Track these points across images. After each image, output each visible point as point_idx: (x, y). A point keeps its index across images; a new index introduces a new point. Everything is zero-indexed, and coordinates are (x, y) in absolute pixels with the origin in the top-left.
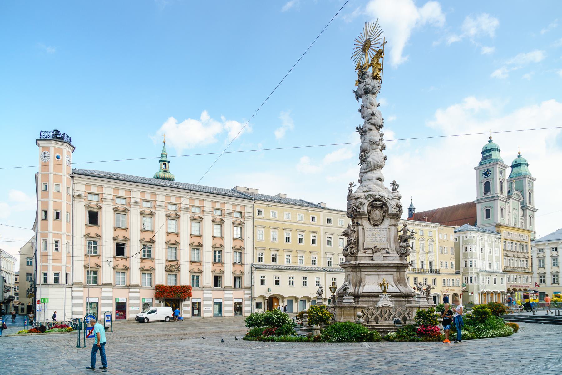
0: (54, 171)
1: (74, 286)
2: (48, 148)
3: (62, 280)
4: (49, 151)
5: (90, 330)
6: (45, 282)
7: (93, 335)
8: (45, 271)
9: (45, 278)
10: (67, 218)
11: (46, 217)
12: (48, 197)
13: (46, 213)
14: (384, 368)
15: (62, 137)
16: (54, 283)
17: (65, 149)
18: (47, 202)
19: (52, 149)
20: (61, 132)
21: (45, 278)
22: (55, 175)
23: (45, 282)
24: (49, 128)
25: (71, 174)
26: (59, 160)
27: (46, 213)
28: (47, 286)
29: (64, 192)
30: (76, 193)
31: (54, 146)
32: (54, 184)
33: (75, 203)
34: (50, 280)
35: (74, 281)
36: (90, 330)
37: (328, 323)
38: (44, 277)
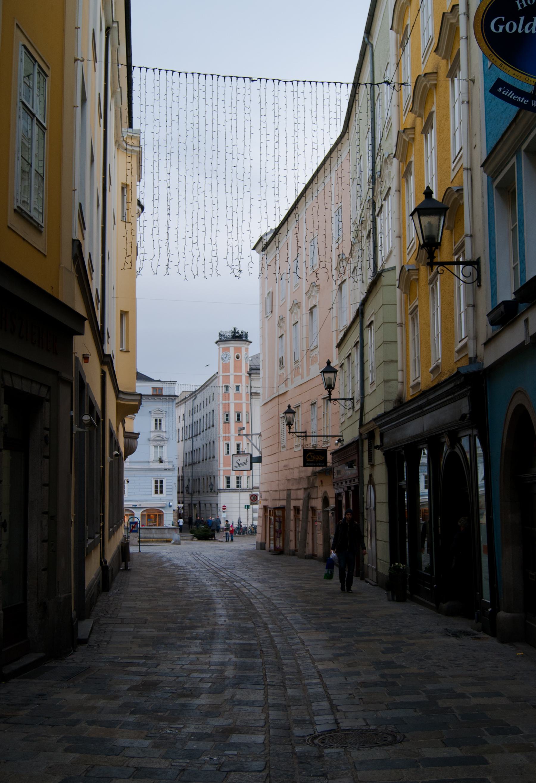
0: (235, 371)
1: (254, 490)
2: (228, 349)
3: (233, 485)
4: (229, 352)
5: (134, 525)
6: (228, 486)
7: (136, 529)
8: (228, 475)
9: (228, 483)
10: (247, 419)
11: (227, 419)
12: (229, 399)
13: (227, 415)
14: (425, 660)
15: (241, 335)
16: (227, 487)
17: (242, 345)
18: (229, 404)
19: (232, 350)
20: (240, 329)
21: (228, 483)
22: (235, 376)
23: (228, 486)
24: (228, 330)
25: (249, 370)
26: (239, 359)
27: (227, 415)
28: (231, 491)
29: (244, 390)
30: (254, 390)
31: (232, 346)
32: (235, 384)
33: (253, 400)
34: (233, 485)
35: (254, 485)
36: (134, 525)
37: (348, 515)
38: (227, 482)
